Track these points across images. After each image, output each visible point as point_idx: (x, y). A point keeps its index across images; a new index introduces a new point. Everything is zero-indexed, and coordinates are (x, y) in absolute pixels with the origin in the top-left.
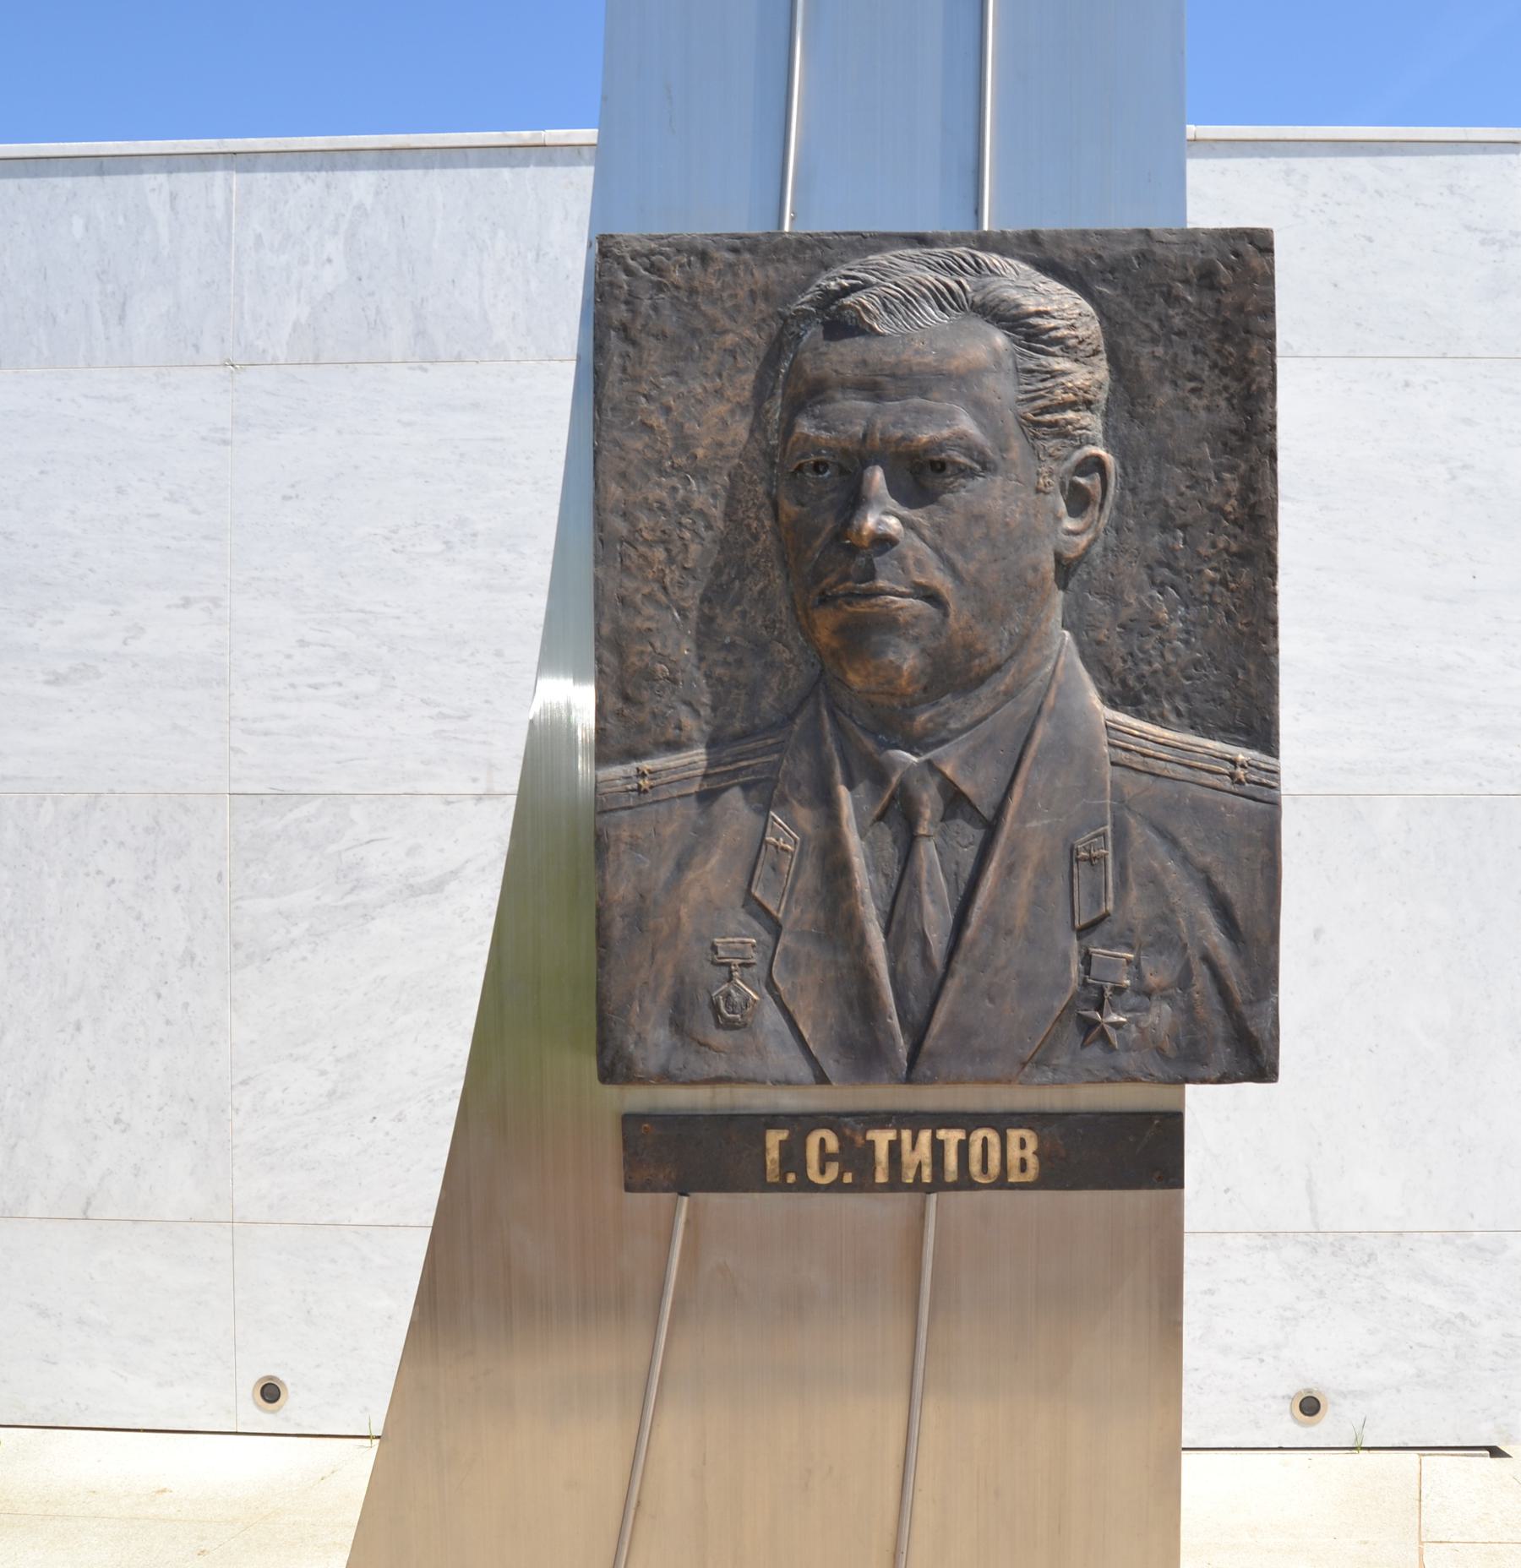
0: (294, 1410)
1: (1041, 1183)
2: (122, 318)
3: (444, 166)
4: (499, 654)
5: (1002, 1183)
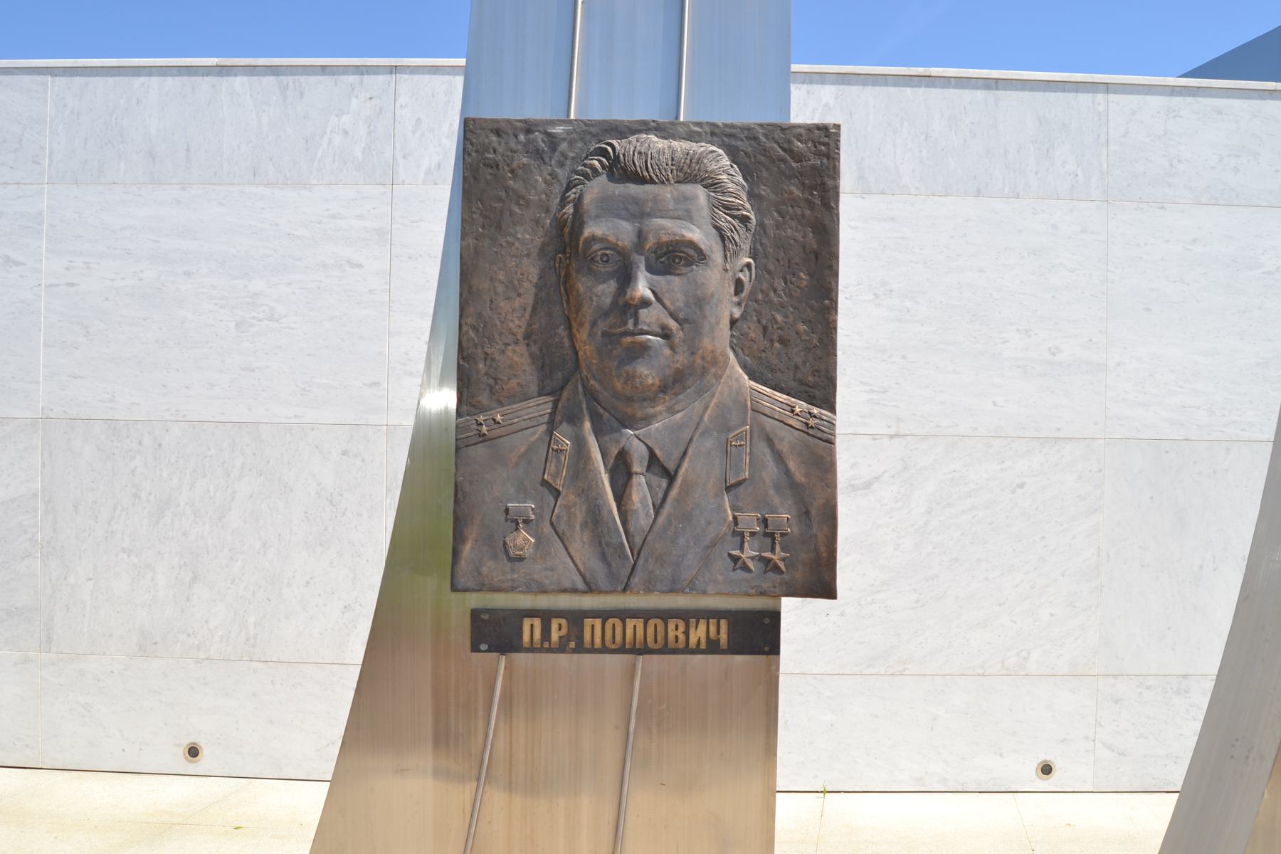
3: (874, 85)
4: (904, 357)
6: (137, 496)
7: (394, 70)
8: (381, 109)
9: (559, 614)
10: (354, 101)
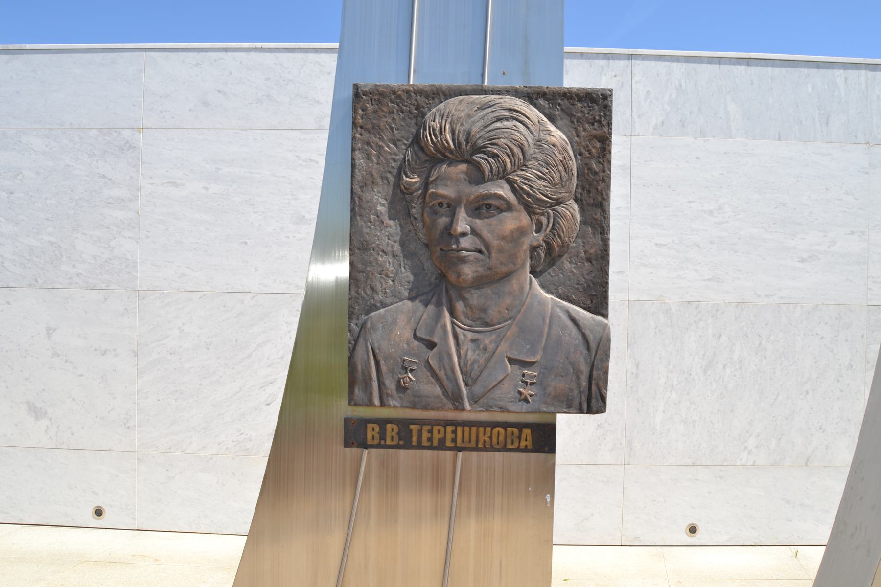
0: (107, 519)
2: (827, 124)
7: (631, 57)
8: (622, 83)
10: (604, 77)
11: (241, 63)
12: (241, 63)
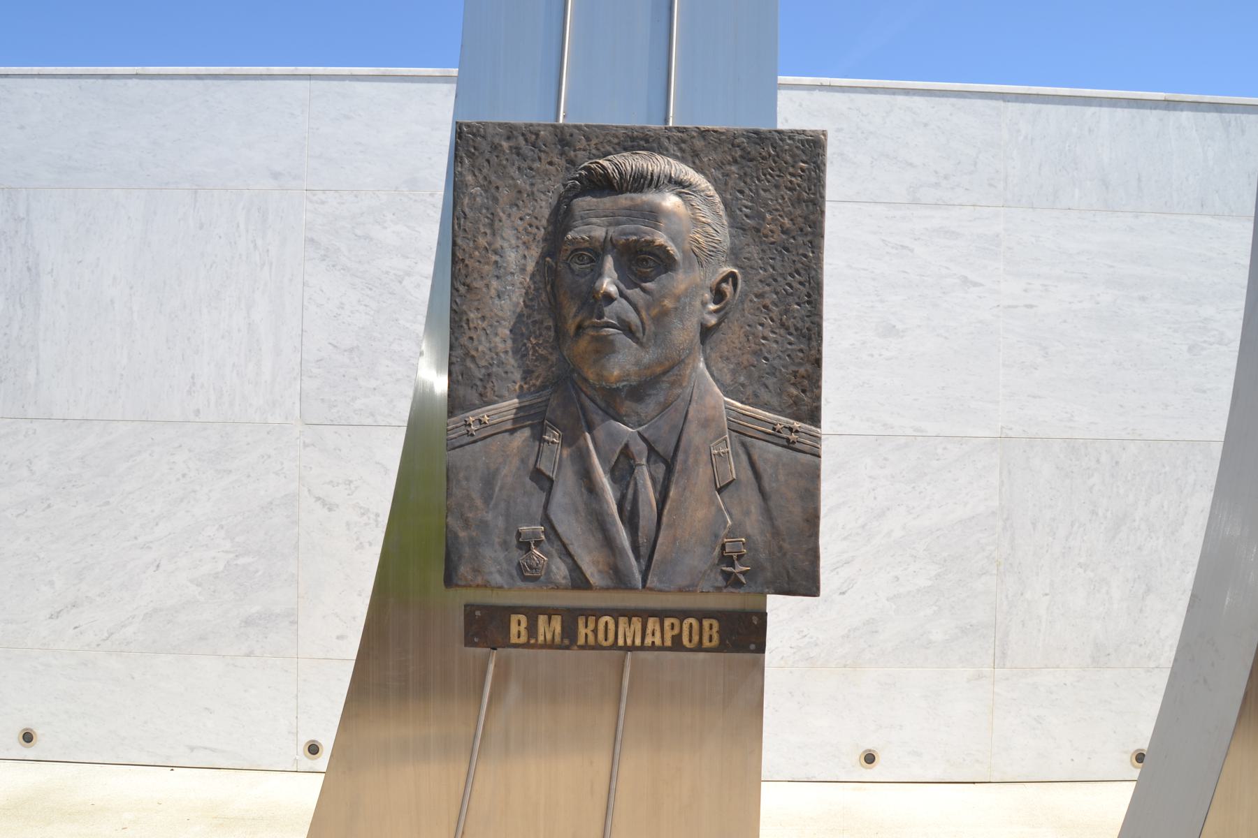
1: (720, 649)
5: (699, 648)
6: (1094, 513)
9: (550, 612)
11: (801, 105)
12: (801, 105)
